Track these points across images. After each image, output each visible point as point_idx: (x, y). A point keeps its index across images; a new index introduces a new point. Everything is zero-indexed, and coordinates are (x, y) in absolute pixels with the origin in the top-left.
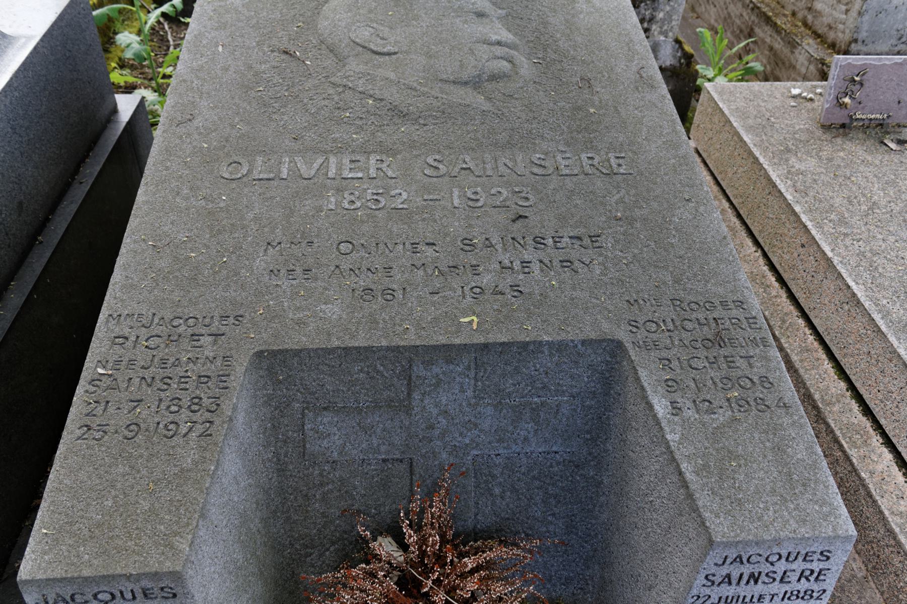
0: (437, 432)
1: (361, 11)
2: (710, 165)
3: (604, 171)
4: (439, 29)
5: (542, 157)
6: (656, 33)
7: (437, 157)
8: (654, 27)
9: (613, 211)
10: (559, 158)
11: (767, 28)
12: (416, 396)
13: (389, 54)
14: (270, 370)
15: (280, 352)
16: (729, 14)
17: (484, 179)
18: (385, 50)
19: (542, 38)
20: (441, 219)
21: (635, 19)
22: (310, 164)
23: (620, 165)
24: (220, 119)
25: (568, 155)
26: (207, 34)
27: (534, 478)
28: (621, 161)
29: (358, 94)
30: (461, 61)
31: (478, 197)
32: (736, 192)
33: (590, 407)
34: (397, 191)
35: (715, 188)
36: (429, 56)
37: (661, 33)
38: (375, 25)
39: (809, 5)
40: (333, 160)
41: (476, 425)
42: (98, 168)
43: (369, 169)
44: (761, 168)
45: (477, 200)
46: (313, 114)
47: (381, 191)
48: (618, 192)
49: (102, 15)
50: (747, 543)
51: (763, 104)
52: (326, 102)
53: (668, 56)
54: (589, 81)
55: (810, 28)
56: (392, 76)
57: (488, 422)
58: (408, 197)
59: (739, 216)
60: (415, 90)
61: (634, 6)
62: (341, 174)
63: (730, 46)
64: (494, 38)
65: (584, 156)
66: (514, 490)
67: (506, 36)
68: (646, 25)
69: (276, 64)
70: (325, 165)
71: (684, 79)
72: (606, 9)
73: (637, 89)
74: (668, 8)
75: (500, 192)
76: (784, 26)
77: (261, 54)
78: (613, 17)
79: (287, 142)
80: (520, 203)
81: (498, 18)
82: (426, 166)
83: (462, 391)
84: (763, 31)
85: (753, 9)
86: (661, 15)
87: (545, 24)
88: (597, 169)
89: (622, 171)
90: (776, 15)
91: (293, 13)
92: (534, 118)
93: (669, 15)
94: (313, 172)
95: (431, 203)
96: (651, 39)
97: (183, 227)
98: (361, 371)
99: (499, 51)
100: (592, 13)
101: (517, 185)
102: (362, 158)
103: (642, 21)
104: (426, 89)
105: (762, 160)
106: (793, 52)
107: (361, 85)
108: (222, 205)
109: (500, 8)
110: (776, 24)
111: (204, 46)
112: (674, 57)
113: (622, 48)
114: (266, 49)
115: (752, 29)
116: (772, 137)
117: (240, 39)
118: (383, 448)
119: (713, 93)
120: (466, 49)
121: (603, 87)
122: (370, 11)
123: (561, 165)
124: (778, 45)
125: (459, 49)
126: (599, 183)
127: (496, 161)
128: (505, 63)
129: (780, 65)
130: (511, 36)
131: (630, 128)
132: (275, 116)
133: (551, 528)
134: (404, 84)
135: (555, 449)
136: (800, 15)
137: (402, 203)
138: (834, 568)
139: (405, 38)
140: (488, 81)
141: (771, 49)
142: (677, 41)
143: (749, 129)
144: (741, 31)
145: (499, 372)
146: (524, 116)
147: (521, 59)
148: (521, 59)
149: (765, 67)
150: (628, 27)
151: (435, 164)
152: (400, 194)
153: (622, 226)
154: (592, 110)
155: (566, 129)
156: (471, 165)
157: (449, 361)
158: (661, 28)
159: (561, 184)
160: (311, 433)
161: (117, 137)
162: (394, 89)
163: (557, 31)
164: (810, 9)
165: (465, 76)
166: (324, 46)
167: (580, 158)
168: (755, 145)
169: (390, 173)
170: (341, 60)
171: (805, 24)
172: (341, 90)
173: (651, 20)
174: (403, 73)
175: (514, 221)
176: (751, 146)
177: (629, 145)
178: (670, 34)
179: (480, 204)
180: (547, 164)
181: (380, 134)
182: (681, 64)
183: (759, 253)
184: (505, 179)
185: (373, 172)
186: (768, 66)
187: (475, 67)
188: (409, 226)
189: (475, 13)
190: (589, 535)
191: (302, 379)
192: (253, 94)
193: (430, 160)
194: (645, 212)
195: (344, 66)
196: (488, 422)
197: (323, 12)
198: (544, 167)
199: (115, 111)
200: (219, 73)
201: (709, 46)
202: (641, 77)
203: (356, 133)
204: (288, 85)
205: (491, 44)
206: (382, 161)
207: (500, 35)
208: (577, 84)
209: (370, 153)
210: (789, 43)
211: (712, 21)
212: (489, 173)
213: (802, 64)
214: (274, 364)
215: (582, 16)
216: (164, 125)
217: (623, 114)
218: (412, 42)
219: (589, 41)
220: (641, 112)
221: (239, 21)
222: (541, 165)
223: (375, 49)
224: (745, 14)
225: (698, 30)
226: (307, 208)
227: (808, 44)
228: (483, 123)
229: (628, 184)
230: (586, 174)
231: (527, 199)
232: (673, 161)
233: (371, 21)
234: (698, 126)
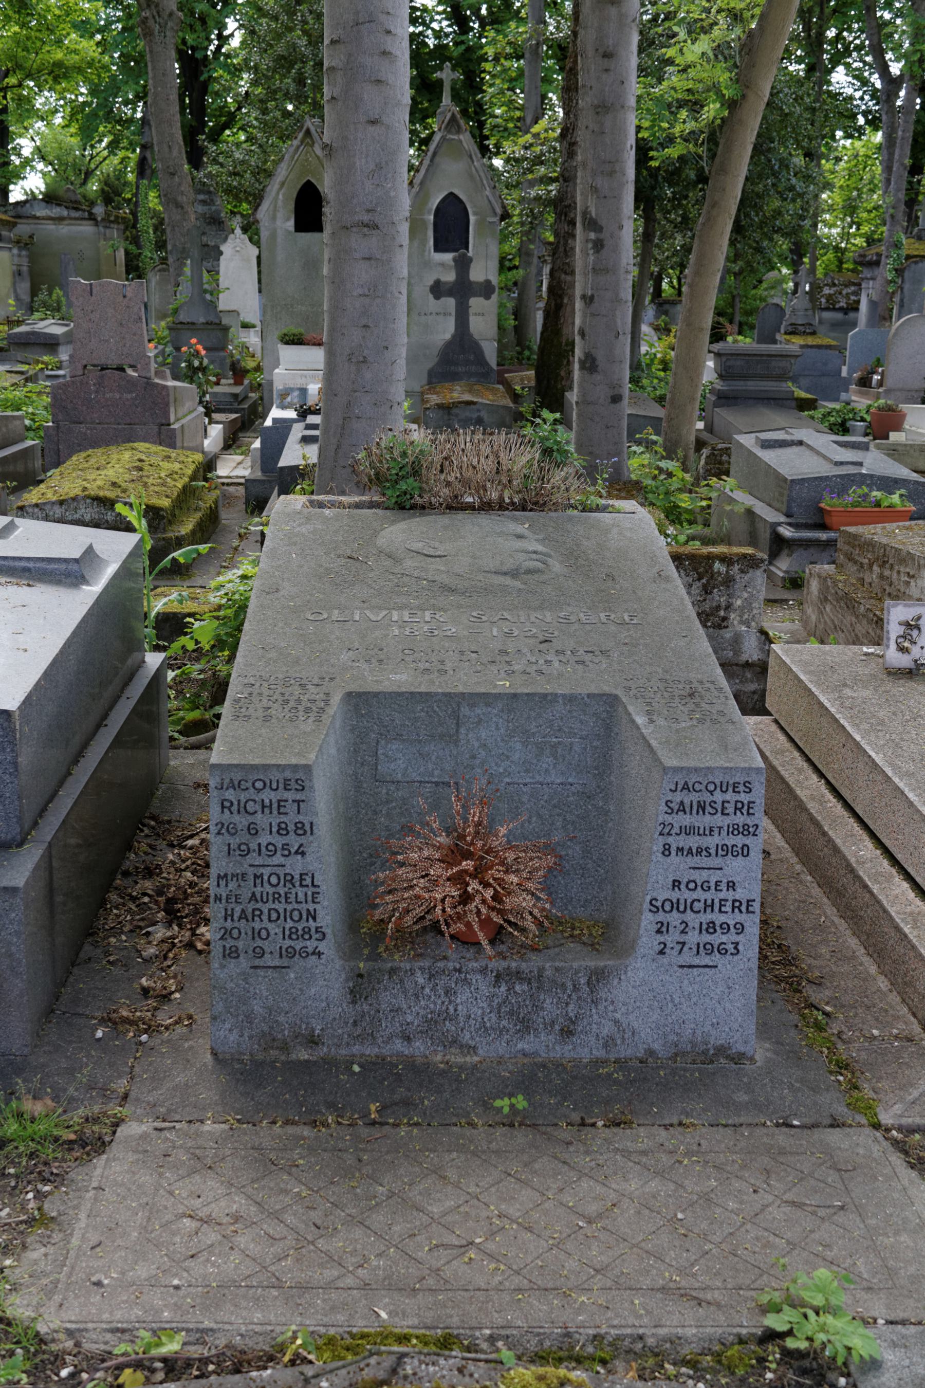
0: (478, 762)
6: (736, 622)
8: (732, 616)
12: (463, 731)
14: (356, 707)
15: (365, 693)
27: (555, 806)
33: (596, 748)
37: (742, 622)
41: (508, 757)
50: (689, 770)
57: (517, 755)
66: (539, 816)
83: (498, 729)
86: (739, 602)
98: (422, 710)
102: (419, 613)
118: (436, 773)
133: (570, 852)
135: (570, 780)
138: (758, 801)
145: (525, 716)
157: (488, 705)
160: (382, 757)
161: (148, 680)
162: (444, 576)
165: (505, 569)
190: (602, 860)
191: (378, 714)
193: (474, 614)
196: (517, 755)
214: (359, 701)
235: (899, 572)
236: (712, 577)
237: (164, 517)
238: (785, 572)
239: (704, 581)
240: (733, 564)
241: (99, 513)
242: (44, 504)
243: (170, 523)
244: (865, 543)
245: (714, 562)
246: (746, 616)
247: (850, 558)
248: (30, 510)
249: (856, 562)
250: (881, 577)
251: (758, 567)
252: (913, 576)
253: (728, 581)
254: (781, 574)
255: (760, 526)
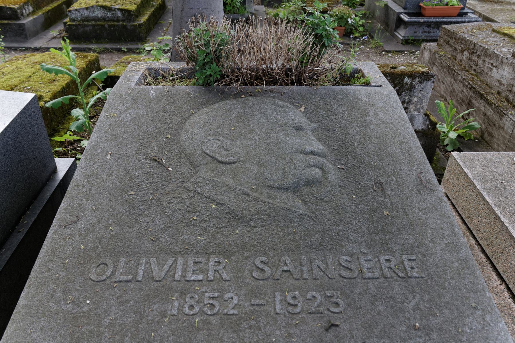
1: (212, 127)
2: (459, 210)
3: (401, 274)
4: (268, 142)
5: (349, 259)
6: (412, 110)
7: (264, 259)
8: (411, 106)
9: (412, 319)
10: (362, 260)
11: (481, 101)
13: (230, 163)
16: (454, 89)
17: (302, 282)
18: (227, 160)
19: (344, 147)
20: (265, 326)
21: (399, 101)
22: (161, 265)
23: (412, 268)
24: (98, 221)
25: (369, 257)
26: (101, 144)
28: (413, 264)
29: (204, 199)
30: (284, 169)
31: (296, 302)
32: (481, 235)
34: (230, 295)
35: (463, 227)
36: (260, 165)
37: (415, 110)
38: (221, 138)
39: (510, 89)
40: (180, 261)
42: (33, 219)
43: (208, 271)
44: (503, 224)
45: (296, 306)
46: (169, 216)
47: (216, 295)
48: (414, 298)
49: (58, 102)
51: (495, 170)
52: (179, 206)
53: (420, 123)
54: (381, 184)
55: (511, 103)
56: (231, 182)
58: (239, 301)
59: (484, 252)
60: (248, 195)
61: (398, 94)
62: (185, 277)
63: (458, 112)
64: (309, 149)
65: (382, 258)
67: (318, 146)
68: (405, 105)
69: (147, 170)
70: (173, 268)
71: (431, 137)
72: (389, 121)
73: (419, 192)
74: (420, 95)
75: (314, 297)
76: (493, 101)
77: (137, 161)
78: (394, 128)
79: (146, 243)
80: (332, 309)
81: (311, 130)
82: (254, 268)
84: (478, 103)
85: (470, 88)
86: (416, 99)
87: (346, 134)
88: (394, 272)
89: (415, 274)
90: (487, 93)
91: (164, 127)
92: (341, 220)
93: (421, 100)
94: (163, 274)
95: (257, 308)
96: (409, 113)
97: (49, 334)
99: (313, 160)
100: (379, 124)
101: (328, 289)
103: (403, 103)
104: (256, 194)
105: (503, 218)
106: (501, 119)
107: (207, 190)
108: (86, 309)
109: (313, 122)
110: (487, 99)
111: (97, 155)
112: (424, 124)
113: (404, 155)
114: (142, 157)
115: (470, 101)
116: (507, 198)
117: (124, 149)
119: (459, 161)
120: (288, 159)
121: (393, 191)
122: (219, 127)
123: (364, 267)
124: (490, 113)
125: (283, 159)
126: (397, 289)
127: (311, 263)
128: (317, 171)
129: (492, 125)
130: (321, 147)
131: (418, 230)
132: (140, 219)
134: (240, 190)
136: (504, 94)
137: (233, 308)
139: (243, 149)
140: (304, 186)
141: (485, 114)
142: (426, 115)
143: (489, 191)
144: (463, 101)
146: (332, 219)
147: (329, 166)
148: (329, 166)
149: (481, 125)
150: (407, 137)
151: (262, 266)
152: (232, 298)
153: (420, 337)
154: (386, 213)
155: (366, 231)
156: (291, 267)
158: (415, 107)
159: (365, 288)
162: (232, 195)
163: (355, 140)
164: (510, 91)
165: (286, 183)
166: (183, 155)
167: (379, 261)
168: (495, 205)
169: (225, 276)
170: (195, 167)
171: (508, 100)
172: (191, 194)
173: (409, 102)
174: (240, 180)
175: (327, 330)
176: (493, 206)
177: (418, 247)
178: (422, 110)
179: (298, 310)
180: (353, 267)
181: (219, 236)
182: (429, 129)
183: (503, 287)
184: (319, 281)
185: (211, 275)
186: (483, 125)
187: (294, 175)
188: (238, 335)
189: (295, 127)
192: (126, 197)
193: (257, 262)
194: (439, 320)
195: (196, 172)
197: (185, 127)
198: (350, 269)
199: (55, 171)
200: (104, 177)
201: (444, 113)
202: (421, 181)
203: (200, 235)
204: (153, 189)
205: (306, 154)
206: (219, 262)
207: (313, 146)
208: (373, 188)
209: (210, 254)
210: (498, 112)
211: (442, 93)
212: (306, 276)
213: (509, 127)
215: (372, 127)
216: (58, 220)
217: (410, 216)
218: (248, 153)
219: (379, 148)
220: (424, 214)
221: (126, 133)
222: (347, 268)
223: (220, 159)
224: (465, 91)
225: (436, 102)
226: (155, 313)
227: (512, 114)
228: (300, 225)
229: (422, 289)
230: (385, 278)
231: (337, 304)
232: (456, 264)
233: (219, 135)
234: (448, 180)
235: (484, 61)
236: (402, 86)
237: (133, 15)
238: (403, 37)
239: (397, 88)
240: (415, 79)
241: (104, 13)
242: (80, 9)
243: (137, 17)
244: (460, 38)
245: (404, 78)
246: (418, 107)
247: (448, 43)
248: (74, 12)
249: (452, 46)
250: (470, 59)
251: (430, 80)
252: (496, 67)
253: (412, 88)
254: (401, 38)
255: (391, 13)
